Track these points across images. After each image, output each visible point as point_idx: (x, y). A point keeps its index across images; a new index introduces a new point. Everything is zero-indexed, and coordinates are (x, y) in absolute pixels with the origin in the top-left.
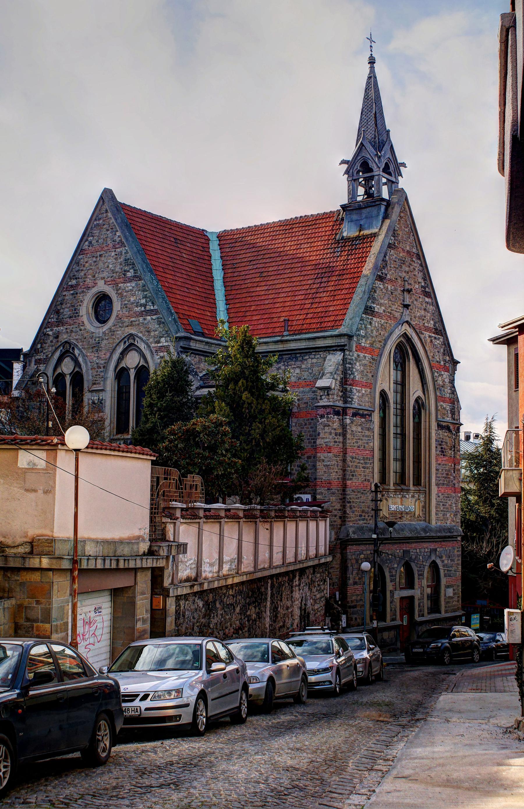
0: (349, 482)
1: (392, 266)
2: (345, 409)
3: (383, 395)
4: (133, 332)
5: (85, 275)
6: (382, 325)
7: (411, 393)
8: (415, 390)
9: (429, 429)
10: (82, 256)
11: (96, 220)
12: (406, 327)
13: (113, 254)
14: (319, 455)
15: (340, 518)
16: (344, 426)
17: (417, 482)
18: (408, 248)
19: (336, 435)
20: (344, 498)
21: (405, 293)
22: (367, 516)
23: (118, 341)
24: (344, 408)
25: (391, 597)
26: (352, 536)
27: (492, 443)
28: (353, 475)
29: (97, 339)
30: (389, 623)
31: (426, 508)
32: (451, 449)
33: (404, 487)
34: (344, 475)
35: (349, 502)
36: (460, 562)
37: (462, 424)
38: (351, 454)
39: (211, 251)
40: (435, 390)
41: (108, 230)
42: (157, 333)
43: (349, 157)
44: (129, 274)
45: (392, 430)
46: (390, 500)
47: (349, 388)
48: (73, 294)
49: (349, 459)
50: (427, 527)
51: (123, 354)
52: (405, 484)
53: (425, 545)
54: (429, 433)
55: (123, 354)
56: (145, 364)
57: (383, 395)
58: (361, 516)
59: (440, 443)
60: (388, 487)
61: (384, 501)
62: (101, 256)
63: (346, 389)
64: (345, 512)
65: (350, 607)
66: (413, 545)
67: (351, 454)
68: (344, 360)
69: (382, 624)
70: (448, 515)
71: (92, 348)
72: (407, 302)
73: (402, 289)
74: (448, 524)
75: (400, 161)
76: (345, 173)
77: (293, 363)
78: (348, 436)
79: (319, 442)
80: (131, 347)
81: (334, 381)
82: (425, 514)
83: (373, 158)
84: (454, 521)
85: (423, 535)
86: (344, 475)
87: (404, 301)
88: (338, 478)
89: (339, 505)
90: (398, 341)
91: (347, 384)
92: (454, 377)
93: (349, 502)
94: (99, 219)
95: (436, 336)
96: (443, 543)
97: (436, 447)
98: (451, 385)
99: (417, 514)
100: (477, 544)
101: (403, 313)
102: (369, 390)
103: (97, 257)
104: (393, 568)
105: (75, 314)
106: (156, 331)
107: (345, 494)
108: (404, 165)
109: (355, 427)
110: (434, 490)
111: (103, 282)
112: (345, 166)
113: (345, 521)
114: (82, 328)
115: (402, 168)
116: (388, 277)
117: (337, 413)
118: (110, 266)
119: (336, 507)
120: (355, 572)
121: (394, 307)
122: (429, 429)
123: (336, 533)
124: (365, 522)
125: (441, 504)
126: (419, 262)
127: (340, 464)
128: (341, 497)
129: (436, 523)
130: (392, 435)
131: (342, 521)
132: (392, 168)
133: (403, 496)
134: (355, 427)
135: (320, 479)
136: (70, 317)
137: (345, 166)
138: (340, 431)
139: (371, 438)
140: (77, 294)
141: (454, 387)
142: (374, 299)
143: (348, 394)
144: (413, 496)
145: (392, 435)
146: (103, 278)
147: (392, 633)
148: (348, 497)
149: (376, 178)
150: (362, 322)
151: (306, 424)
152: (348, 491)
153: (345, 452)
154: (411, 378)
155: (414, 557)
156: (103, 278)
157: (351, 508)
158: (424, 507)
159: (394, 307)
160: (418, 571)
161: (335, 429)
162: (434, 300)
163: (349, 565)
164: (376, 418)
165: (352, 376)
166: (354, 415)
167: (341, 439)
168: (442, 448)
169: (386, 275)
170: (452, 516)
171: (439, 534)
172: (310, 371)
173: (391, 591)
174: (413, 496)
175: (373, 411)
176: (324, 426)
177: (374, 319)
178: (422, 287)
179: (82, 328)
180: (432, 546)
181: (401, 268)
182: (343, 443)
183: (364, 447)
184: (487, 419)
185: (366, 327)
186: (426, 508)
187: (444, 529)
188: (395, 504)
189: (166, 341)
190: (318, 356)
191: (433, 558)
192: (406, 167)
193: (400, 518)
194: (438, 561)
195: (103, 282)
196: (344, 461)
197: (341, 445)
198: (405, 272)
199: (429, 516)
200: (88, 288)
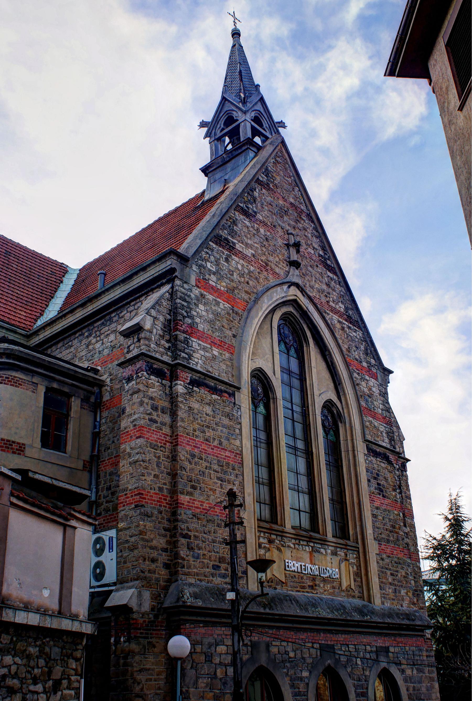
2: (174, 368)
9: (354, 451)
14: (123, 446)
15: (166, 566)
16: (173, 398)
17: (342, 531)
20: (175, 528)
21: (291, 249)
26: (190, 601)
27: (462, 527)
28: (194, 487)
31: (362, 574)
32: (394, 490)
34: (174, 484)
35: (186, 536)
36: (435, 675)
45: (284, 440)
46: (287, 553)
47: (182, 336)
49: (183, 454)
50: (364, 606)
53: (365, 639)
54: (354, 456)
59: (374, 476)
60: (280, 528)
63: (176, 337)
64: (176, 556)
66: (341, 637)
67: (188, 448)
70: (403, 592)
74: (405, 608)
75: (276, 119)
78: (181, 414)
82: (361, 587)
84: (414, 604)
85: (357, 617)
87: (289, 258)
88: (161, 489)
91: (177, 330)
92: (386, 389)
93: (186, 536)
96: (399, 639)
97: (369, 481)
99: (345, 585)
100: (461, 657)
102: (227, 355)
104: (301, 679)
107: (177, 520)
109: (198, 406)
110: (373, 548)
112: (205, 129)
113: (176, 573)
115: (280, 129)
116: (259, 217)
117: (159, 374)
119: (154, 543)
120: (202, 683)
122: (354, 451)
123: (155, 597)
127: (165, 463)
128: (166, 524)
129: (383, 603)
130: (284, 449)
131: (171, 574)
133: (314, 550)
137: (205, 129)
139: (234, 430)
141: (388, 403)
143: (181, 345)
145: (284, 449)
152: (184, 514)
153: (174, 440)
154: (314, 371)
155: (343, 659)
157: (190, 548)
158: (358, 574)
160: (356, 687)
161: (151, 398)
162: (341, 280)
166: (193, 383)
167: (167, 419)
168: (378, 484)
170: (410, 594)
171: (388, 620)
174: (334, 554)
176: (132, 395)
180: (380, 642)
181: (282, 217)
182: (171, 427)
184: (450, 495)
186: (362, 574)
187: (397, 614)
188: (298, 560)
191: (383, 665)
192: (284, 127)
193: (312, 587)
194: (394, 670)
196: (174, 458)
197: (166, 430)
199: (369, 590)
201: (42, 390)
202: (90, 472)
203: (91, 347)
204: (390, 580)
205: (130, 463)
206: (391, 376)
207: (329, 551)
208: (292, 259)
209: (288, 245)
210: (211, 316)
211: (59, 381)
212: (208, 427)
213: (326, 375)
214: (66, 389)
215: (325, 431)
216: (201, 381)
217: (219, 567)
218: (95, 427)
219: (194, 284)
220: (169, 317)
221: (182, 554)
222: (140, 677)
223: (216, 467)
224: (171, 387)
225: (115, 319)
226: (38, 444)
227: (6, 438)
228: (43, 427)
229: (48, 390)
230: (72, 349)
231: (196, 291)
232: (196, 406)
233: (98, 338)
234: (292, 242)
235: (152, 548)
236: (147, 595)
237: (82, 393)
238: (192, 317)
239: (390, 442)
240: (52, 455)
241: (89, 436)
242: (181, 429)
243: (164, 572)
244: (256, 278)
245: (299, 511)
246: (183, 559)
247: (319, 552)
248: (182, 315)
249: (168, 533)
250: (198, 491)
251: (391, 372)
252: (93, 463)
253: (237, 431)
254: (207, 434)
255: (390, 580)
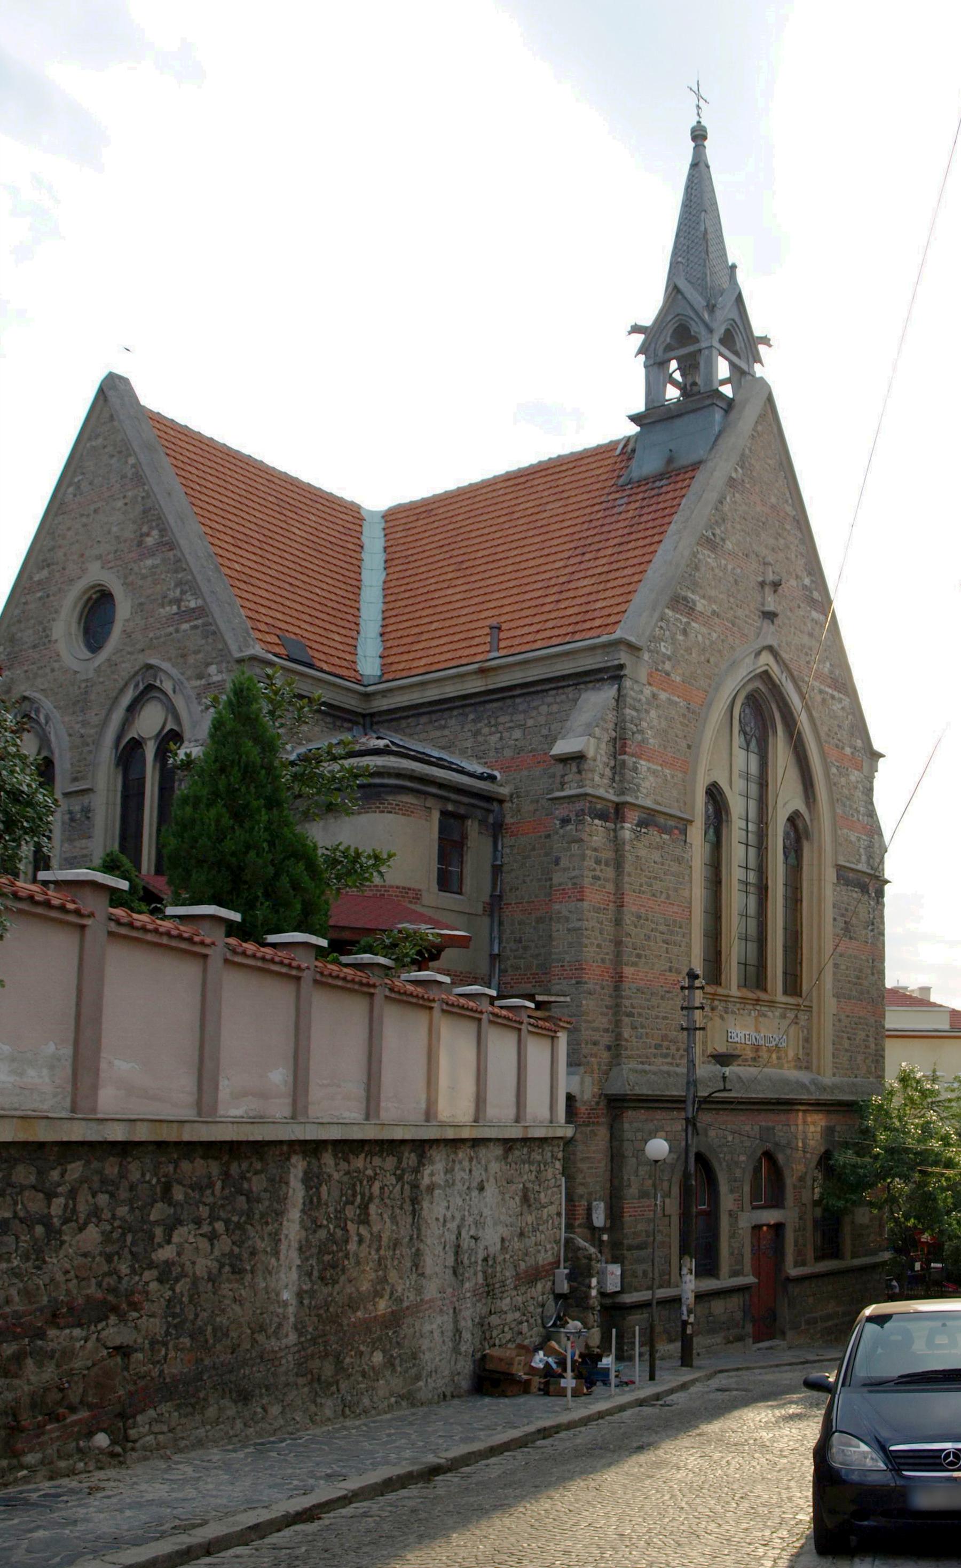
0: (628, 971)
1: (738, 526)
3: (714, 794)
4: (152, 661)
5: (65, 555)
6: (712, 643)
7: (780, 804)
8: (787, 798)
10: (60, 518)
11: (90, 439)
12: (766, 658)
13: (120, 504)
15: (609, 1048)
16: (617, 844)
17: (793, 985)
18: (773, 500)
19: (598, 862)
20: (618, 1005)
22: (673, 1048)
23: (122, 683)
24: (617, 804)
25: (731, 1225)
29: (83, 685)
30: (725, 1281)
33: (763, 996)
34: (618, 955)
35: (630, 1015)
37: (887, 882)
38: (634, 909)
39: (364, 538)
40: (832, 802)
41: (112, 456)
42: (200, 656)
43: (648, 318)
44: (149, 541)
45: (737, 874)
47: (630, 760)
48: (40, 598)
49: (628, 919)
51: (133, 709)
52: (765, 990)
55: (133, 709)
56: (175, 728)
57: (714, 794)
58: (658, 1047)
61: (718, 1020)
62: (96, 511)
64: (619, 1037)
65: (630, 1248)
68: (620, 698)
69: (710, 1284)
71: (74, 704)
72: (770, 607)
73: (760, 579)
75: (758, 332)
76: (640, 352)
77: (507, 718)
78: (628, 868)
79: (557, 878)
80: (148, 692)
81: (592, 740)
83: (699, 325)
86: (618, 955)
87: (763, 605)
89: (605, 1020)
90: (750, 687)
91: (625, 753)
92: (872, 783)
93: (630, 1015)
94: (97, 437)
95: (835, 693)
97: (835, 919)
98: (865, 798)
101: (760, 628)
103: (88, 515)
105: (45, 639)
106: (199, 652)
107: (621, 997)
108: (765, 341)
109: (644, 850)
111: (98, 564)
112: (640, 338)
113: (618, 1056)
114: (56, 665)
115: (762, 348)
116: (729, 545)
117: (603, 816)
118: (114, 529)
119: (595, 1025)
121: (740, 613)
122: (820, 880)
124: (669, 1060)
125: (845, 1035)
126: (799, 535)
127: (609, 928)
130: (736, 885)
132: (742, 342)
134: (644, 850)
135: (559, 960)
136: (35, 647)
137: (640, 338)
138: (608, 855)
140: (48, 596)
141: (872, 803)
142: (695, 584)
144: (783, 1016)
146: (99, 557)
147: (734, 1302)
148: (627, 1002)
149: (706, 352)
150: (663, 624)
151: (534, 849)
152: (628, 988)
156: (99, 557)
159: (740, 613)
161: (595, 850)
163: (628, 1153)
164: (697, 834)
165: (639, 737)
167: (610, 873)
169: (723, 540)
172: (545, 732)
173: (731, 1214)
175: (691, 822)
177: (693, 624)
178: (805, 587)
179: (56, 665)
181: (758, 535)
183: (668, 897)
185: (673, 638)
189: (220, 672)
190: (564, 697)
195: (98, 564)
196: (618, 922)
197: (610, 887)
198: (766, 547)
200: (71, 581)
201: (436, 815)
202: (491, 916)
203: (480, 739)
204: (847, 1046)
205: (568, 930)
206: (881, 760)
207: (777, 1014)
208: (767, 609)
209: (762, 584)
210: (664, 724)
211: (455, 802)
212: (655, 878)
213: (791, 760)
214: (462, 811)
215: (785, 853)
216: (649, 819)
217: (661, 1046)
218: (495, 859)
219: (645, 682)
220: (614, 734)
221: (626, 1035)
222: (583, 1166)
223: (662, 928)
224: (615, 830)
225: (521, 708)
226: (435, 887)
227: (401, 884)
228: (439, 863)
229: (444, 813)
230: (446, 732)
231: (648, 691)
232: (643, 853)
233: (493, 729)
234: (771, 577)
235: (595, 1030)
236: (588, 1080)
237: (479, 813)
238: (641, 732)
239: (868, 864)
240: (448, 899)
241: (488, 868)
242: (627, 886)
243: (605, 1055)
244: (719, 651)
245: (746, 965)
246: (627, 1040)
247: (765, 1016)
248: (631, 730)
249: (610, 1012)
250: (643, 960)
251: (881, 756)
252: (495, 905)
253: (687, 878)
254: (655, 887)
255: (847, 1046)
